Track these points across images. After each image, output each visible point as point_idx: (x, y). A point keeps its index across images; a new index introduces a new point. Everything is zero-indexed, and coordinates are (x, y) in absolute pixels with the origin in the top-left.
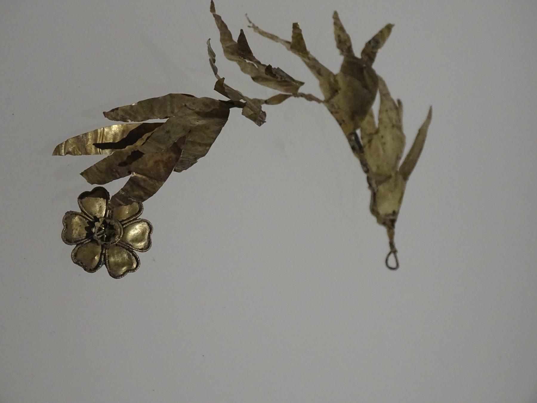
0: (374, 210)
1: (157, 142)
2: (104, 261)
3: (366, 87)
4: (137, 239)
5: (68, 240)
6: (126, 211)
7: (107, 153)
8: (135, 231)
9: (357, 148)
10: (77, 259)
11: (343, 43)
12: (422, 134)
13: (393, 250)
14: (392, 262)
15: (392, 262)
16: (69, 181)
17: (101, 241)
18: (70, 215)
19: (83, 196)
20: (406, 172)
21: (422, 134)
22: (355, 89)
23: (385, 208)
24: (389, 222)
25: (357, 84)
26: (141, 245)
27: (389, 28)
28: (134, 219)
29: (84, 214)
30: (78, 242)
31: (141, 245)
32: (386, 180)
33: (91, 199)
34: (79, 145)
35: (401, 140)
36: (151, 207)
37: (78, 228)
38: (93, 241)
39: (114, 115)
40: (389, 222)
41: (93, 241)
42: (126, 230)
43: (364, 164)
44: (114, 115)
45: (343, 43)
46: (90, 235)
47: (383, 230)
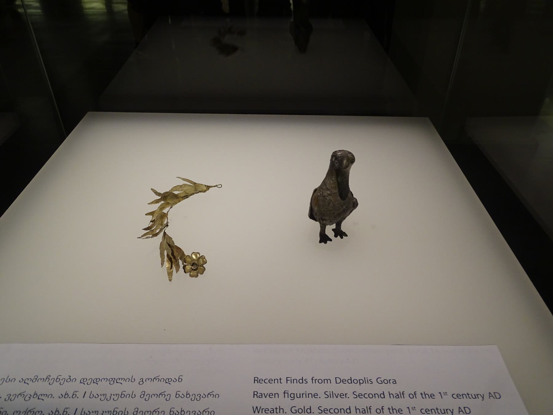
0: (205, 191)
1: (173, 255)
2: (202, 265)
3: (169, 195)
4: (196, 256)
5: (197, 276)
6: (188, 260)
7: (173, 266)
8: (194, 257)
9: (187, 197)
10: (202, 273)
11: (157, 201)
12: (184, 179)
13: (216, 186)
14: (220, 186)
15: (220, 186)
16: (180, 275)
17: (197, 266)
18: (191, 276)
19: (185, 272)
20: (195, 183)
21: (184, 179)
22: (168, 198)
23: (205, 188)
24: (208, 187)
25: (169, 197)
26: (198, 255)
27: (152, 189)
28: (190, 257)
29: (190, 272)
30: (198, 273)
31: (198, 255)
32: (198, 188)
33: (186, 270)
34: (170, 274)
35: (185, 185)
36: (186, 253)
37: (195, 273)
38: (197, 269)
39: (162, 264)
40: (208, 187)
41: (197, 269)
42: (194, 260)
43: (192, 195)
44: (162, 264)
45: (157, 201)
46: (195, 270)
47: (210, 189)
